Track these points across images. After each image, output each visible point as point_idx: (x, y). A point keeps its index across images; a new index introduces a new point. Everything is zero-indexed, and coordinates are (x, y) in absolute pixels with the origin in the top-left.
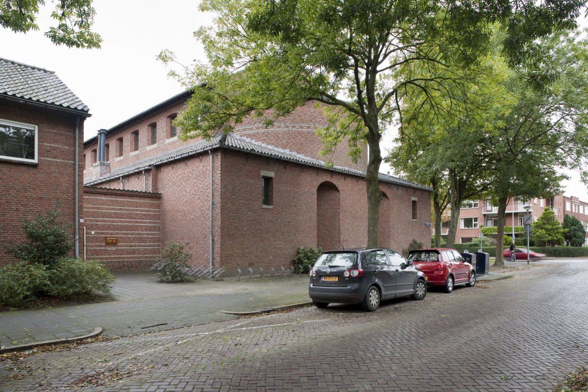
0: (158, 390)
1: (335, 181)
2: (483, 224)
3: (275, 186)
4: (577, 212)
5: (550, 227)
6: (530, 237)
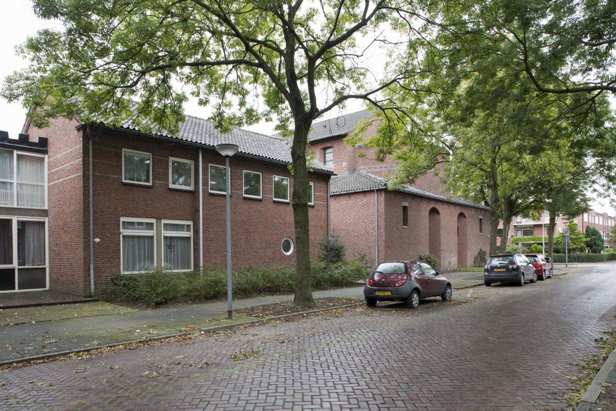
0: (201, 402)
1: (439, 207)
2: (513, 234)
3: (410, 213)
4: (593, 222)
5: (574, 237)
6: (568, 246)
